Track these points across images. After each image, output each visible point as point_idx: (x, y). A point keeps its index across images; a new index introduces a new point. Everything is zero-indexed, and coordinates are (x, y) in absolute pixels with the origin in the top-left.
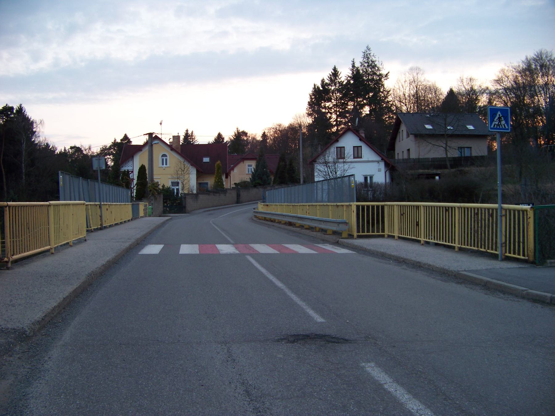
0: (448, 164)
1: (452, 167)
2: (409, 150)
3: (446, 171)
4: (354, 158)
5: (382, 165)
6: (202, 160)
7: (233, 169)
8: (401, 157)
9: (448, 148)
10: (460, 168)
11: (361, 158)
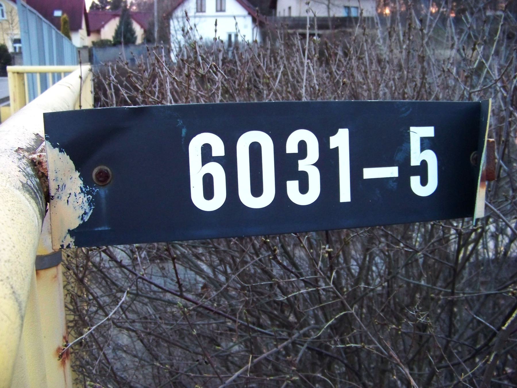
0: (330, 24)
1: (337, 27)
2: (290, 8)
3: (328, 32)
4: (217, 11)
5: (249, 19)
6: (53, 13)
7: (103, 26)
8: (282, 15)
9: (331, 6)
10: (343, 29)
11: (224, 11)
